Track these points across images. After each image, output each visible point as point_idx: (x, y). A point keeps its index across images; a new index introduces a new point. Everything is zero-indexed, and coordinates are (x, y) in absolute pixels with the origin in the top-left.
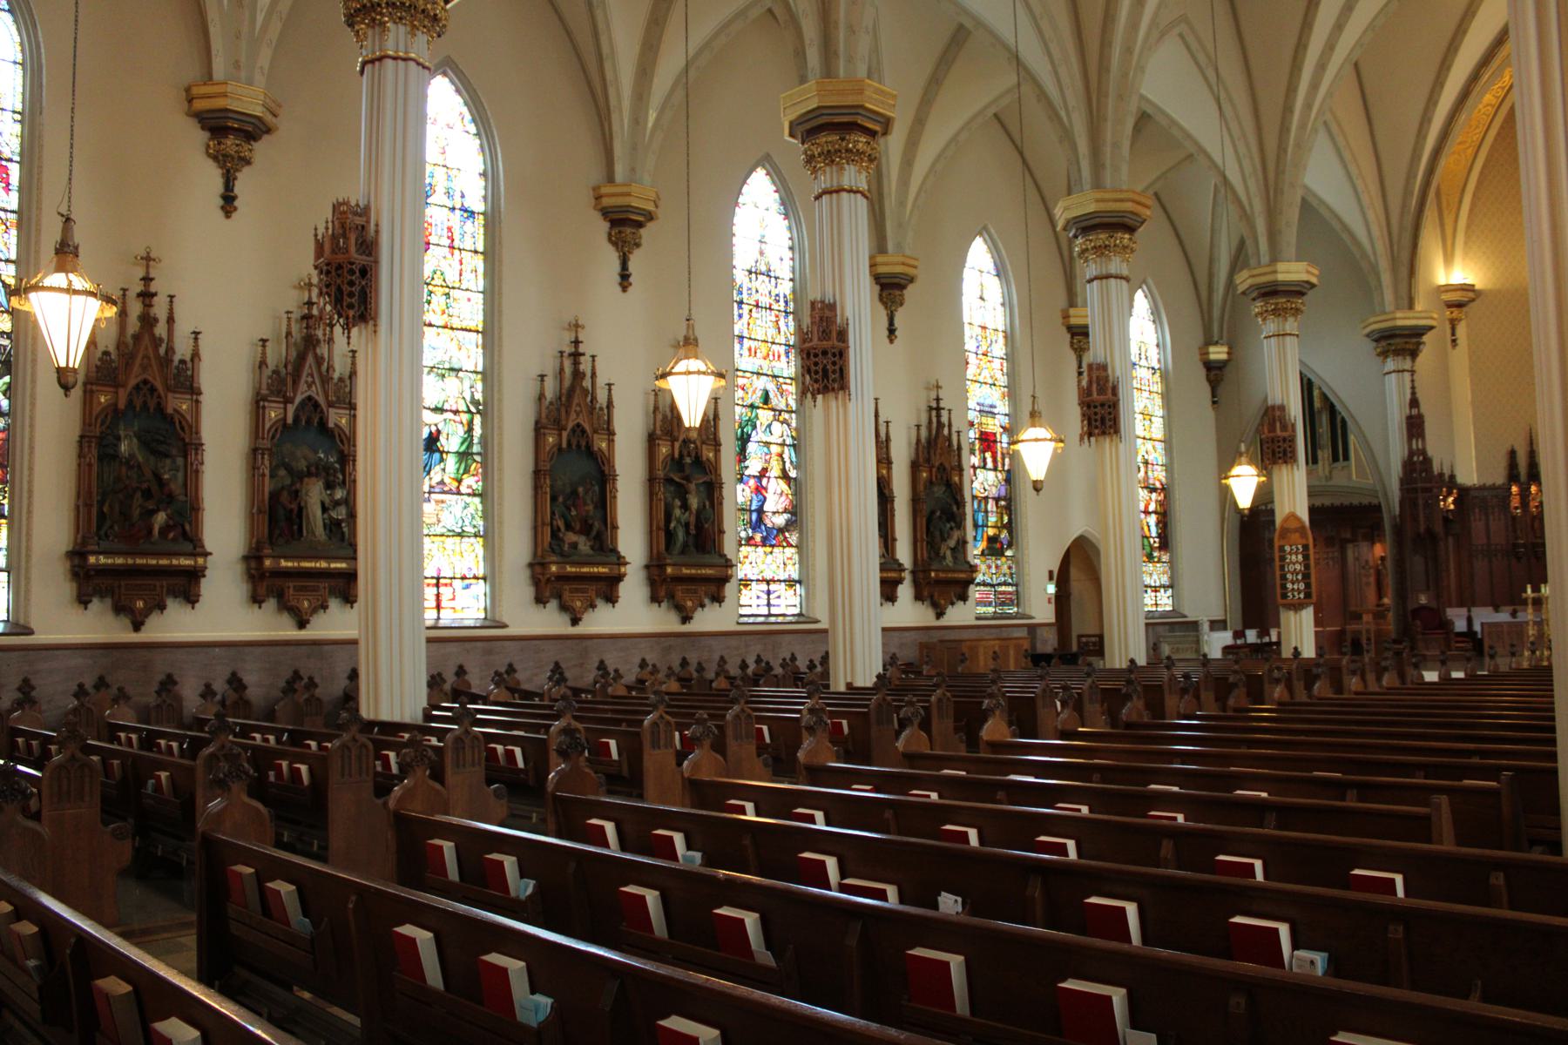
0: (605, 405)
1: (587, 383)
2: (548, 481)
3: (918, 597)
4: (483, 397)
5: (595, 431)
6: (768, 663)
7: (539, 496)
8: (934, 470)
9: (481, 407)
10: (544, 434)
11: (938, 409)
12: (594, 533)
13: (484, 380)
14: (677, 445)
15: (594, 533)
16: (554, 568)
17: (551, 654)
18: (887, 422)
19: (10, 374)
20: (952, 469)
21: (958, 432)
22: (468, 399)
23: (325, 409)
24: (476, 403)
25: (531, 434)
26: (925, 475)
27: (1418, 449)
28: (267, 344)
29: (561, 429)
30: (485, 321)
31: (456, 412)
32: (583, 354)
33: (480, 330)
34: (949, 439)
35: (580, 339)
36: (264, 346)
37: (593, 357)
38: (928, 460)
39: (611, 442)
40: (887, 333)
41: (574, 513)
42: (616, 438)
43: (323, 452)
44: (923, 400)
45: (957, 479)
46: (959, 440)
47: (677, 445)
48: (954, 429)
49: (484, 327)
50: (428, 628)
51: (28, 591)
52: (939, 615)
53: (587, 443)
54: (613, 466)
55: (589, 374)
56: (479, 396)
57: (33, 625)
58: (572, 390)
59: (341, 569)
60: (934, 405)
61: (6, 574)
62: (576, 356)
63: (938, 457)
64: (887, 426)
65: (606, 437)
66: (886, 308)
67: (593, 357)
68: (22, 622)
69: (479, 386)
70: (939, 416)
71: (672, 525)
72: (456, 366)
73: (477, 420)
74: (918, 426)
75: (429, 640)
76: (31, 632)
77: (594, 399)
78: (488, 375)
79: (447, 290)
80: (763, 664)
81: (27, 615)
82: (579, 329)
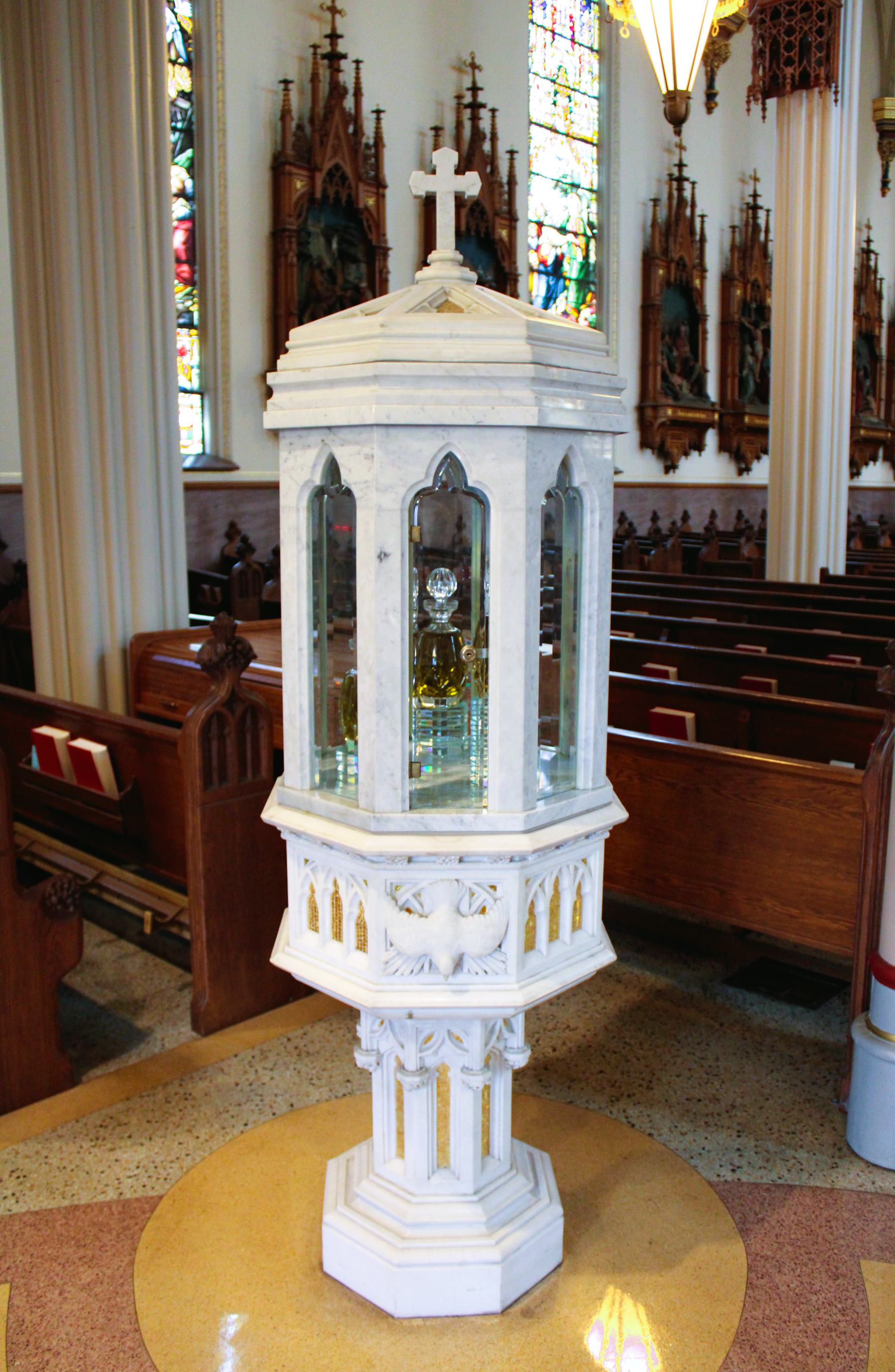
0: (371, 142)
1: (349, 103)
2: (294, 246)
3: (723, 447)
4: (598, 219)
5: (359, 178)
6: (631, 524)
7: (282, 271)
8: (673, 266)
9: (595, 231)
10: (291, 174)
11: (476, 106)
12: (694, 377)
13: (599, 200)
14: (319, 178)
15: (694, 377)
16: (670, 412)
17: (652, 502)
18: (378, 112)
19: (191, 146)
20: (694, 267)
21: (512, 153)
22: (586, 221)
23: (353, 184)
24: (591, 225)
25: (264, 176)
26: (661, 272)
27: (669, 92)
28: (291, 86)
29: (312, 170)
30: (600, 133)
31: (576, 234)
32: (344, 57)
33: (595, 142)
34: (356, 118)
35: (479, 85)
36: (286, 89)
37: (358, 62)
38: (666, 251)
39: (380, 198)
40: (878, 184)
41: (675, 354)
42: (388, 192)
43: (483, 269)
44: (739, 195)
45: (504, 233)
46: (702, 229)
47: (319, 178)
48: (698, 212)
49: (599, 139)
50: (186, 470)
51: (227, 419)
52: (670, 467)
53: (487, 228)
54: (384, 235)
55: (351, 91)
56: (594, 219)
57: (236, 459)
58: (329, 110)
59: (700, 419)
60: (750, 200)
61: (198, 397)
62: (334, 58)
63: (329, 150)
64: (378, 119)
65: (374, 190)
66: (882, 158)
67: (358, 62)
68: (222, 454)
69: (594, 207)
70: (475, 118)
71: (745, 372)
72: (576, 182)
73: (593, 244)
74: (656, 201)
75: (189, 488)
76: (232, 468)
77: (359, 131)
78: (602, 195)
79: (569, 92)
80: (626, 526)
81: (227, 444)
82: (338, 17)
